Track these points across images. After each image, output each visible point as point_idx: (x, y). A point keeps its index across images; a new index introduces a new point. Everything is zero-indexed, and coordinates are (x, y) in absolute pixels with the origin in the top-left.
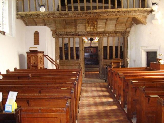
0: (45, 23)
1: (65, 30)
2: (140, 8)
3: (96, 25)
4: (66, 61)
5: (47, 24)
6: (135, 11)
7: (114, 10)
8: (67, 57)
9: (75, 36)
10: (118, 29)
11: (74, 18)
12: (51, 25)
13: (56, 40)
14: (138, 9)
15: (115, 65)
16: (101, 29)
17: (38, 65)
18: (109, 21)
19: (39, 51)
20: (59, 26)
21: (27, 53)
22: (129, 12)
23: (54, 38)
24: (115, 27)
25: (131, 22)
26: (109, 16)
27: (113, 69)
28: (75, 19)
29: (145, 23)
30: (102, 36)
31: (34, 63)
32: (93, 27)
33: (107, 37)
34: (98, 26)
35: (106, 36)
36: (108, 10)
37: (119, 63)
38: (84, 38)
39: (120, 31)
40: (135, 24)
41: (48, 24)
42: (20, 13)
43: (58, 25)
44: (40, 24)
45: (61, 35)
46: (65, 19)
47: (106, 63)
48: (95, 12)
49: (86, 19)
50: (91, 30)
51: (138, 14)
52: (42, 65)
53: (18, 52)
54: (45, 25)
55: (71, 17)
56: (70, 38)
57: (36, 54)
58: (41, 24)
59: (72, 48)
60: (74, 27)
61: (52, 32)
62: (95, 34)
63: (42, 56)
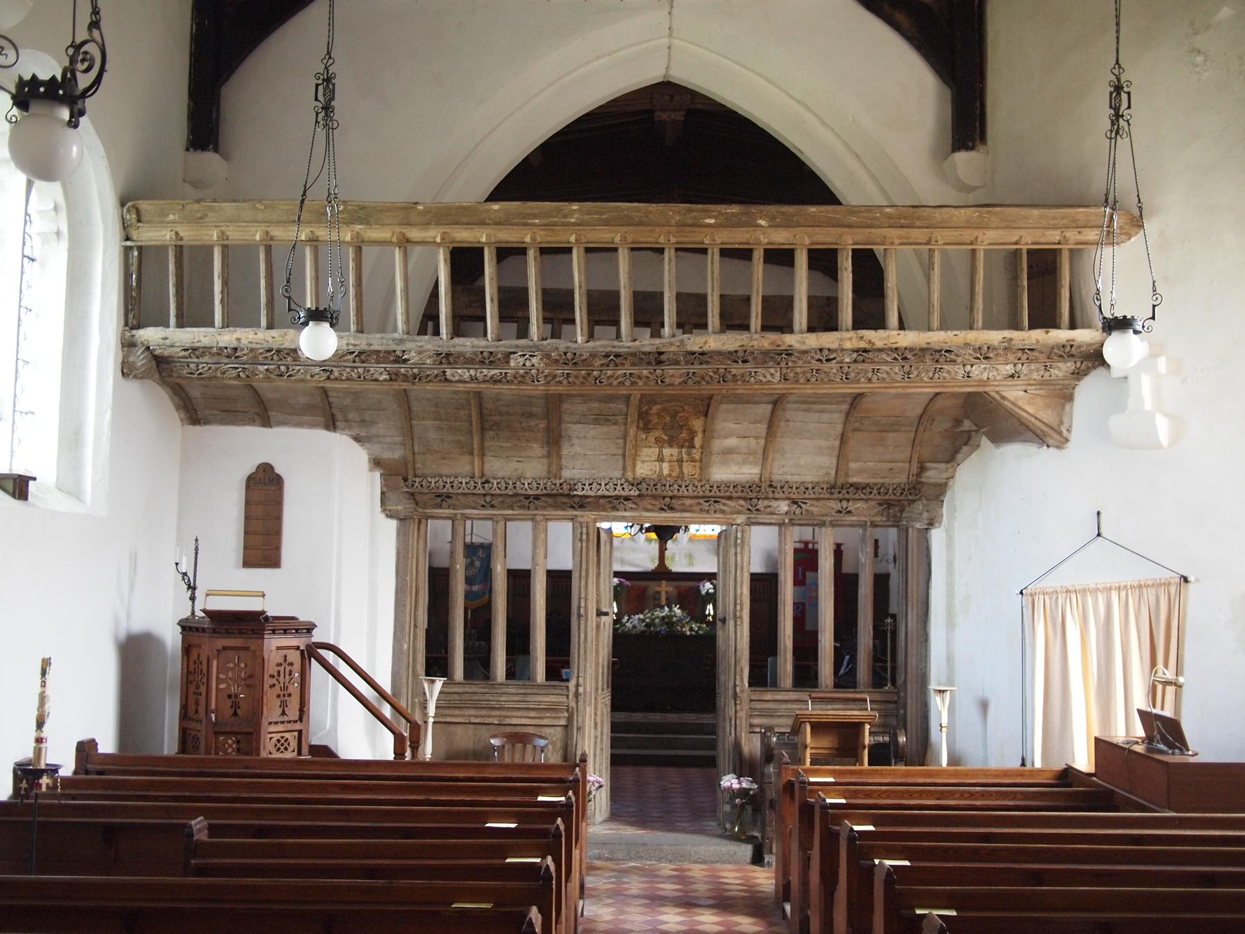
0: (334, 411)
1: (476, 459)
2: (1016, 326)
3: (700, 435)
4: (477, 688)
5: (347, 421)
6: (984, 354)
7: (827, 340)
8: (479, 664)
9: (544, 508)
10: (860, 472)
11: (539, 389)
12: (373, 423)
13: (402, 535)
14: (1008, 334)
15: (827, 742)
16: (735, 468)
17: (264, 722)
18: (795, 416)
19: (269, 614)
20: (431, 435)
21: (188, 627)
22: (941, 355)
23: (390, 516)
24: (842, 456)
25: (958, 422)
26: (797, 382)
27: (806, 771)
28: (547, 397)
29: (1060, 433)
30: (739, 513)
31: (235, 706)
32: (675, 451)
33: (781, 525)
34: (718, 444)
35: (774, 519)
36: (790, 340)
37: (856, 727)
38: (619, 528)
39: (872, 481)
40: (985, 441)
41: (352, 415)
42: (150, 335)
43: (427, 428)
44: (297, 419)
45: (443, 498)
46: (479, 395)
47: (770, 714)
48: (693, 353)
49: (628, 397)
50: (666, 472)
51: (1009, 369)
52: (290, 727)
53: (117, 623)
54: (331, 424)
55: (521, 379)
56: (507, 519)
57: (253, 644)
58: (305, 418)
59: (520, 580)
60: (538, 450)
61: (377, 475)
62: (688, 502)
63: (295, 657)
